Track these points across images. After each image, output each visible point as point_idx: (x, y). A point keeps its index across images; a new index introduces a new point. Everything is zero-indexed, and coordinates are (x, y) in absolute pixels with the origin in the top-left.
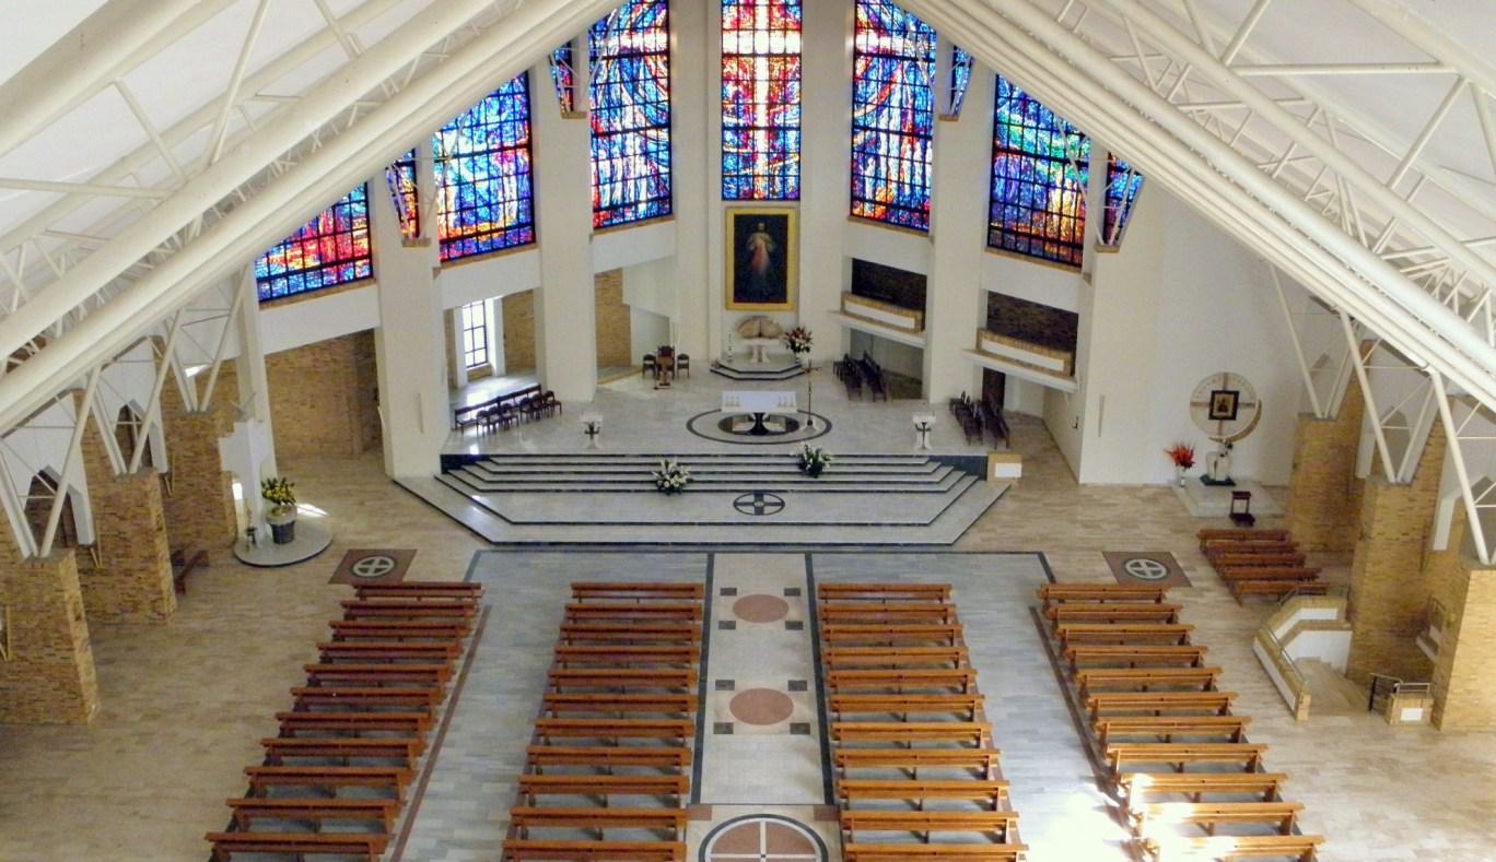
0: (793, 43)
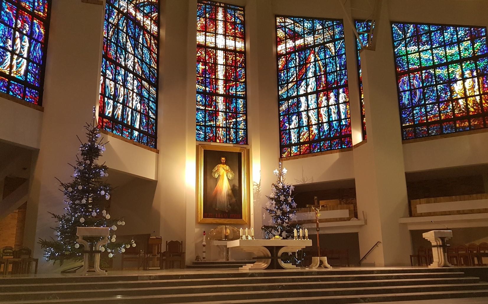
0: (240, 45)
